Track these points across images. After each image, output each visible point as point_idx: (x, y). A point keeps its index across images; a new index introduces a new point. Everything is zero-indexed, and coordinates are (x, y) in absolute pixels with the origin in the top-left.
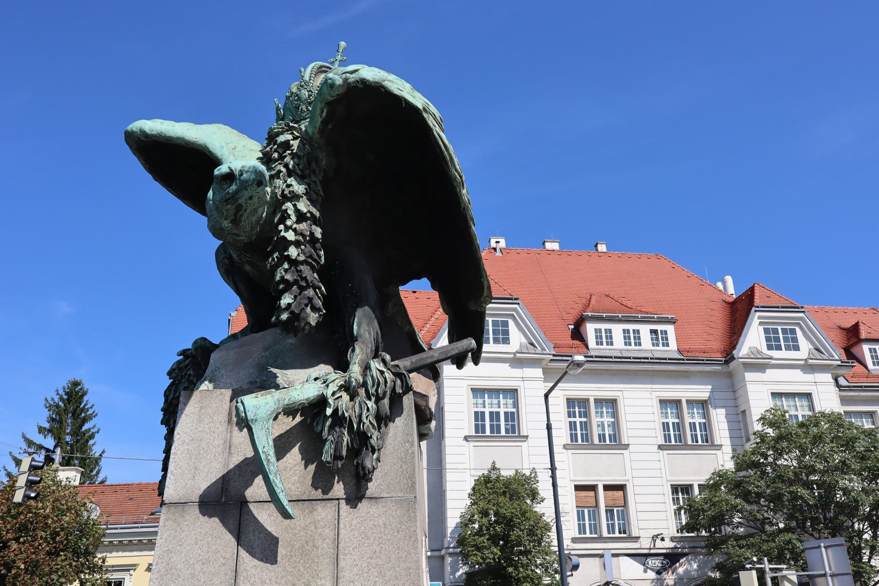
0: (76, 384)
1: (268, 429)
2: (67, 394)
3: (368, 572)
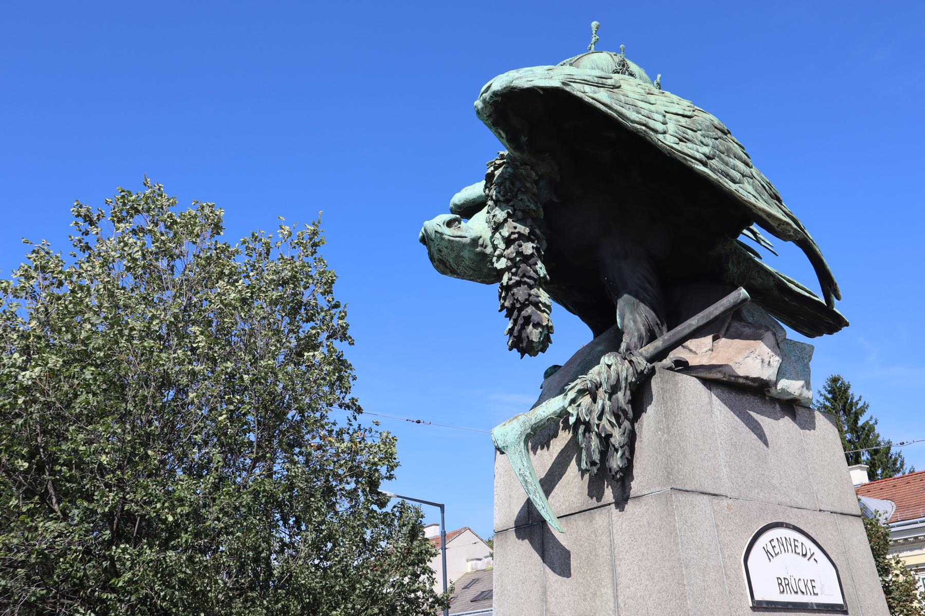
0: (835, 380)
1: (520, 451)
2: (830, 392)
3: (640, 576)
